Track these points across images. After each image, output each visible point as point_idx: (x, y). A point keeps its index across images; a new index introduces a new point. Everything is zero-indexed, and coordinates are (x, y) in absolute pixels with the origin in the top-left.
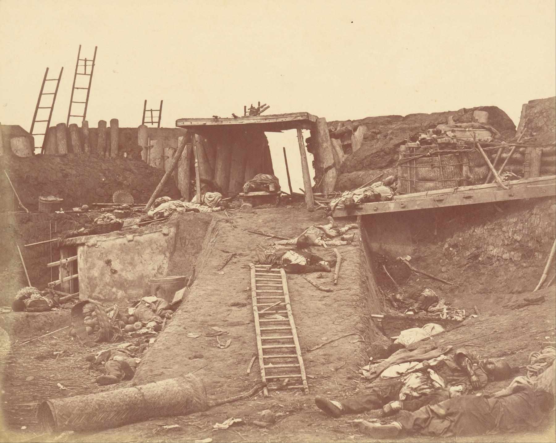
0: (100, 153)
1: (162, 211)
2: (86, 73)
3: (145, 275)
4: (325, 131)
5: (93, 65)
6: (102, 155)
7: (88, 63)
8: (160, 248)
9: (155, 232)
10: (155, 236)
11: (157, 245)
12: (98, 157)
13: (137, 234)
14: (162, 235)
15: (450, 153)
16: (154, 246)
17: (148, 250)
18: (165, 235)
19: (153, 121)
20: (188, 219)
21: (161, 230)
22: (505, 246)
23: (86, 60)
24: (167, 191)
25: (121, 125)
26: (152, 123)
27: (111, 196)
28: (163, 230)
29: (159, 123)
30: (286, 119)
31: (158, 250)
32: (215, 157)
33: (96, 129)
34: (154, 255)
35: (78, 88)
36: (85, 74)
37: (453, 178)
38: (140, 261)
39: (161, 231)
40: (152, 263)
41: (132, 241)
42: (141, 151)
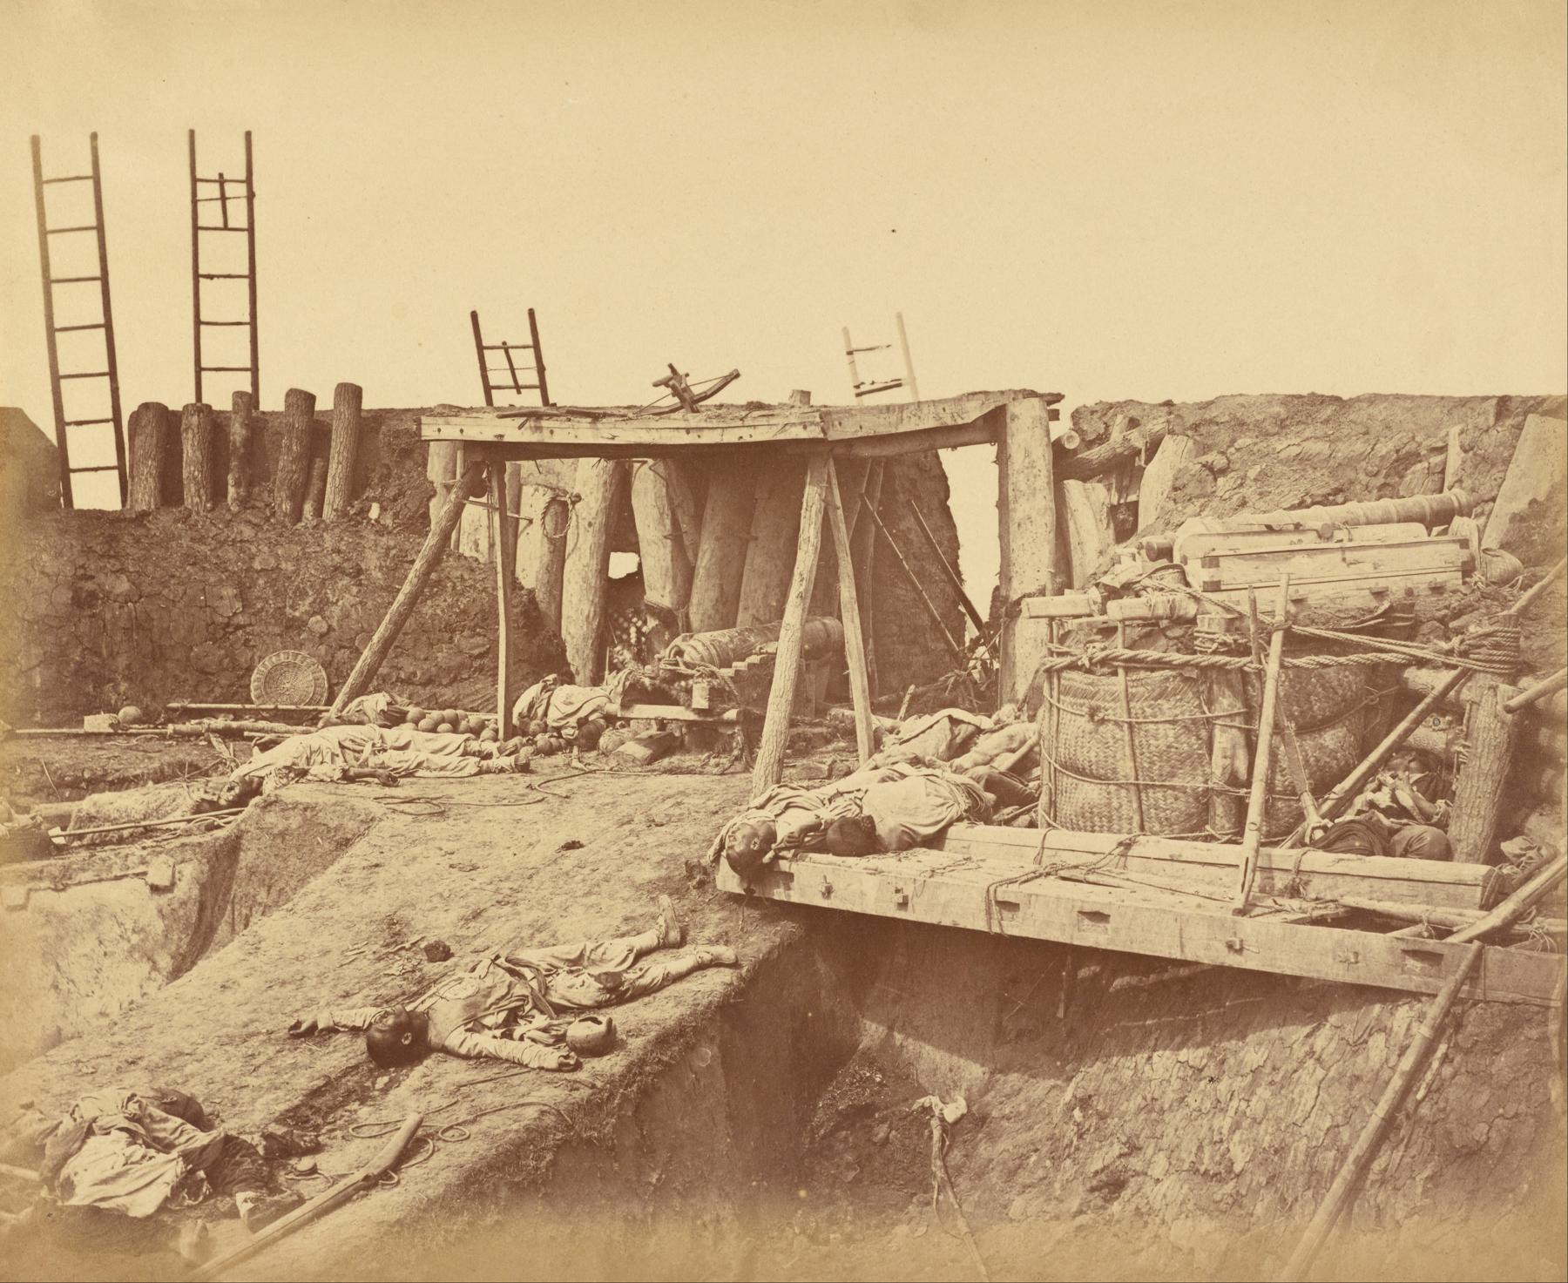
0: (280, 506)
1: (262, 773)
2: (231, 225)
3: (68, 1030)
4: (1027, 454)
5: (251, 196)
6: (286, 515)
7: (231, 189)
8: (135, 939)
9: (117, 878)
10: (112, 893)
11: (121, 924)
12: (267, 520)
13: (46, 884)
14: (147, 890)
15: (1159, 665)
16: (110, 930)
17: (88, 944)
18: (155, 889)
19: (521, 383)
20: (281, 827)
21: (141, 869)
22: (1198, 1179)
23: (222, 181)
24: (476, 652)
25: (369, 403)
26: (518, 388)
27: (249, 670)
28: (151, 870)
29: (543, 387)
30: (751, 431)
31: (126, 946)
32: (698, 520)
33: (281, 413)
34: (107, 962)
35: (211, 277)
36: (226, 228)
37: (1172, 775)
38: (48, 981)
39: (145, 873)
40: (98, 993)
41: (23, 907)
42: (429, 499)
